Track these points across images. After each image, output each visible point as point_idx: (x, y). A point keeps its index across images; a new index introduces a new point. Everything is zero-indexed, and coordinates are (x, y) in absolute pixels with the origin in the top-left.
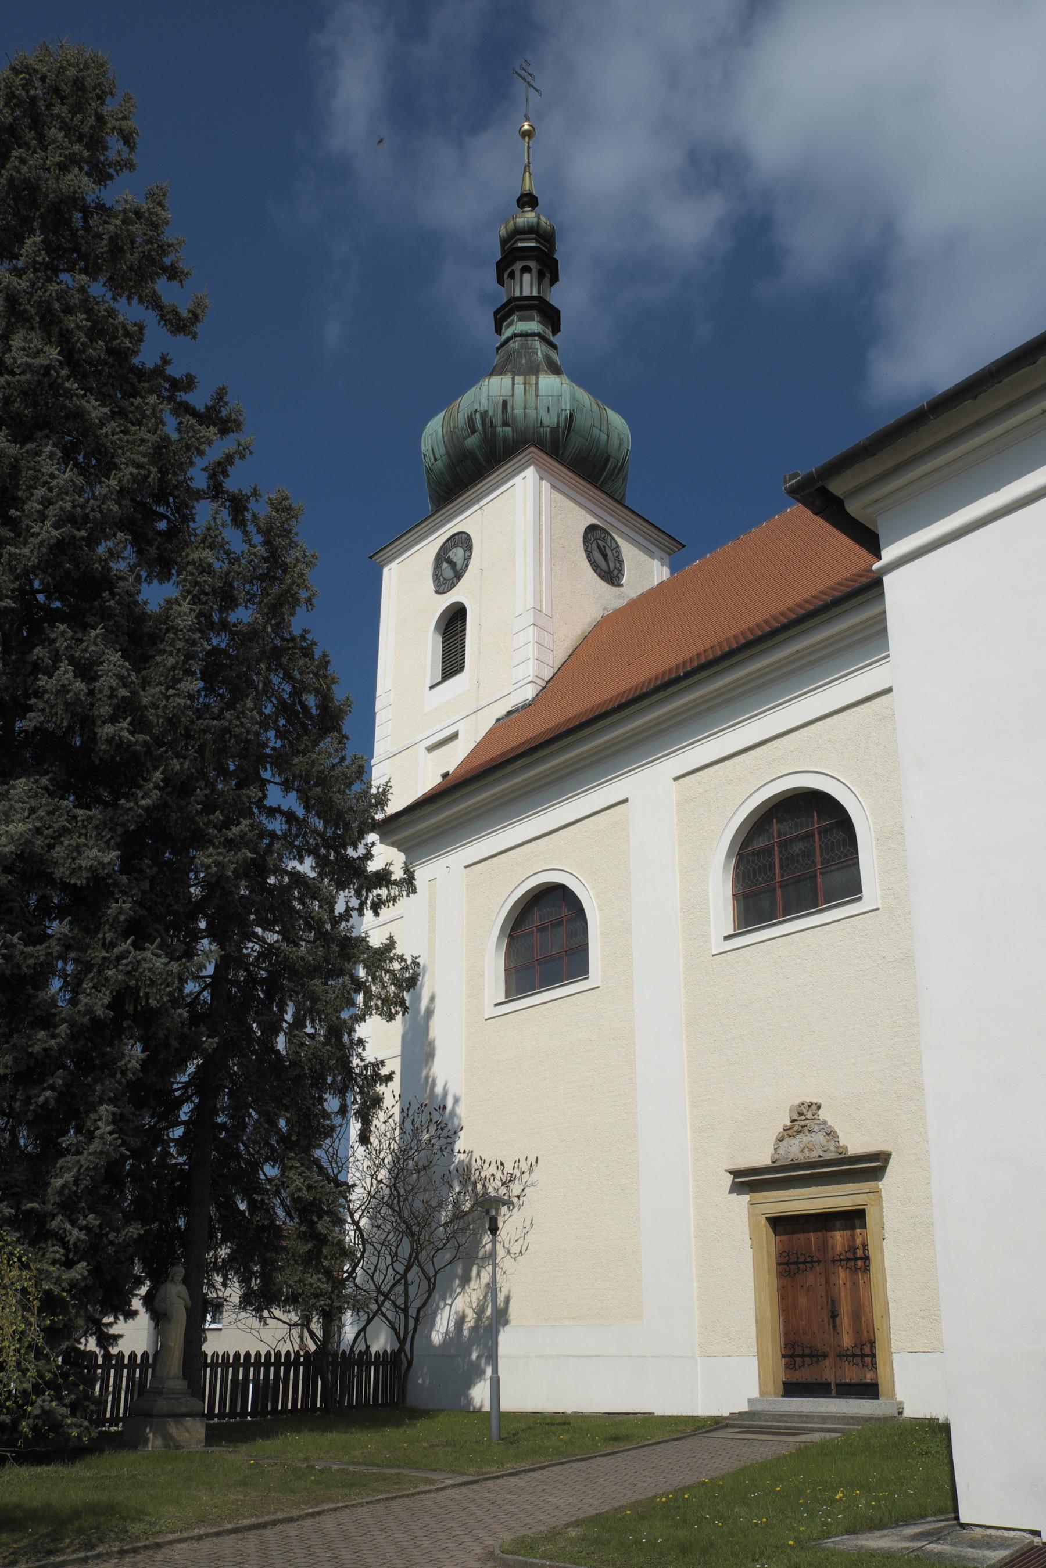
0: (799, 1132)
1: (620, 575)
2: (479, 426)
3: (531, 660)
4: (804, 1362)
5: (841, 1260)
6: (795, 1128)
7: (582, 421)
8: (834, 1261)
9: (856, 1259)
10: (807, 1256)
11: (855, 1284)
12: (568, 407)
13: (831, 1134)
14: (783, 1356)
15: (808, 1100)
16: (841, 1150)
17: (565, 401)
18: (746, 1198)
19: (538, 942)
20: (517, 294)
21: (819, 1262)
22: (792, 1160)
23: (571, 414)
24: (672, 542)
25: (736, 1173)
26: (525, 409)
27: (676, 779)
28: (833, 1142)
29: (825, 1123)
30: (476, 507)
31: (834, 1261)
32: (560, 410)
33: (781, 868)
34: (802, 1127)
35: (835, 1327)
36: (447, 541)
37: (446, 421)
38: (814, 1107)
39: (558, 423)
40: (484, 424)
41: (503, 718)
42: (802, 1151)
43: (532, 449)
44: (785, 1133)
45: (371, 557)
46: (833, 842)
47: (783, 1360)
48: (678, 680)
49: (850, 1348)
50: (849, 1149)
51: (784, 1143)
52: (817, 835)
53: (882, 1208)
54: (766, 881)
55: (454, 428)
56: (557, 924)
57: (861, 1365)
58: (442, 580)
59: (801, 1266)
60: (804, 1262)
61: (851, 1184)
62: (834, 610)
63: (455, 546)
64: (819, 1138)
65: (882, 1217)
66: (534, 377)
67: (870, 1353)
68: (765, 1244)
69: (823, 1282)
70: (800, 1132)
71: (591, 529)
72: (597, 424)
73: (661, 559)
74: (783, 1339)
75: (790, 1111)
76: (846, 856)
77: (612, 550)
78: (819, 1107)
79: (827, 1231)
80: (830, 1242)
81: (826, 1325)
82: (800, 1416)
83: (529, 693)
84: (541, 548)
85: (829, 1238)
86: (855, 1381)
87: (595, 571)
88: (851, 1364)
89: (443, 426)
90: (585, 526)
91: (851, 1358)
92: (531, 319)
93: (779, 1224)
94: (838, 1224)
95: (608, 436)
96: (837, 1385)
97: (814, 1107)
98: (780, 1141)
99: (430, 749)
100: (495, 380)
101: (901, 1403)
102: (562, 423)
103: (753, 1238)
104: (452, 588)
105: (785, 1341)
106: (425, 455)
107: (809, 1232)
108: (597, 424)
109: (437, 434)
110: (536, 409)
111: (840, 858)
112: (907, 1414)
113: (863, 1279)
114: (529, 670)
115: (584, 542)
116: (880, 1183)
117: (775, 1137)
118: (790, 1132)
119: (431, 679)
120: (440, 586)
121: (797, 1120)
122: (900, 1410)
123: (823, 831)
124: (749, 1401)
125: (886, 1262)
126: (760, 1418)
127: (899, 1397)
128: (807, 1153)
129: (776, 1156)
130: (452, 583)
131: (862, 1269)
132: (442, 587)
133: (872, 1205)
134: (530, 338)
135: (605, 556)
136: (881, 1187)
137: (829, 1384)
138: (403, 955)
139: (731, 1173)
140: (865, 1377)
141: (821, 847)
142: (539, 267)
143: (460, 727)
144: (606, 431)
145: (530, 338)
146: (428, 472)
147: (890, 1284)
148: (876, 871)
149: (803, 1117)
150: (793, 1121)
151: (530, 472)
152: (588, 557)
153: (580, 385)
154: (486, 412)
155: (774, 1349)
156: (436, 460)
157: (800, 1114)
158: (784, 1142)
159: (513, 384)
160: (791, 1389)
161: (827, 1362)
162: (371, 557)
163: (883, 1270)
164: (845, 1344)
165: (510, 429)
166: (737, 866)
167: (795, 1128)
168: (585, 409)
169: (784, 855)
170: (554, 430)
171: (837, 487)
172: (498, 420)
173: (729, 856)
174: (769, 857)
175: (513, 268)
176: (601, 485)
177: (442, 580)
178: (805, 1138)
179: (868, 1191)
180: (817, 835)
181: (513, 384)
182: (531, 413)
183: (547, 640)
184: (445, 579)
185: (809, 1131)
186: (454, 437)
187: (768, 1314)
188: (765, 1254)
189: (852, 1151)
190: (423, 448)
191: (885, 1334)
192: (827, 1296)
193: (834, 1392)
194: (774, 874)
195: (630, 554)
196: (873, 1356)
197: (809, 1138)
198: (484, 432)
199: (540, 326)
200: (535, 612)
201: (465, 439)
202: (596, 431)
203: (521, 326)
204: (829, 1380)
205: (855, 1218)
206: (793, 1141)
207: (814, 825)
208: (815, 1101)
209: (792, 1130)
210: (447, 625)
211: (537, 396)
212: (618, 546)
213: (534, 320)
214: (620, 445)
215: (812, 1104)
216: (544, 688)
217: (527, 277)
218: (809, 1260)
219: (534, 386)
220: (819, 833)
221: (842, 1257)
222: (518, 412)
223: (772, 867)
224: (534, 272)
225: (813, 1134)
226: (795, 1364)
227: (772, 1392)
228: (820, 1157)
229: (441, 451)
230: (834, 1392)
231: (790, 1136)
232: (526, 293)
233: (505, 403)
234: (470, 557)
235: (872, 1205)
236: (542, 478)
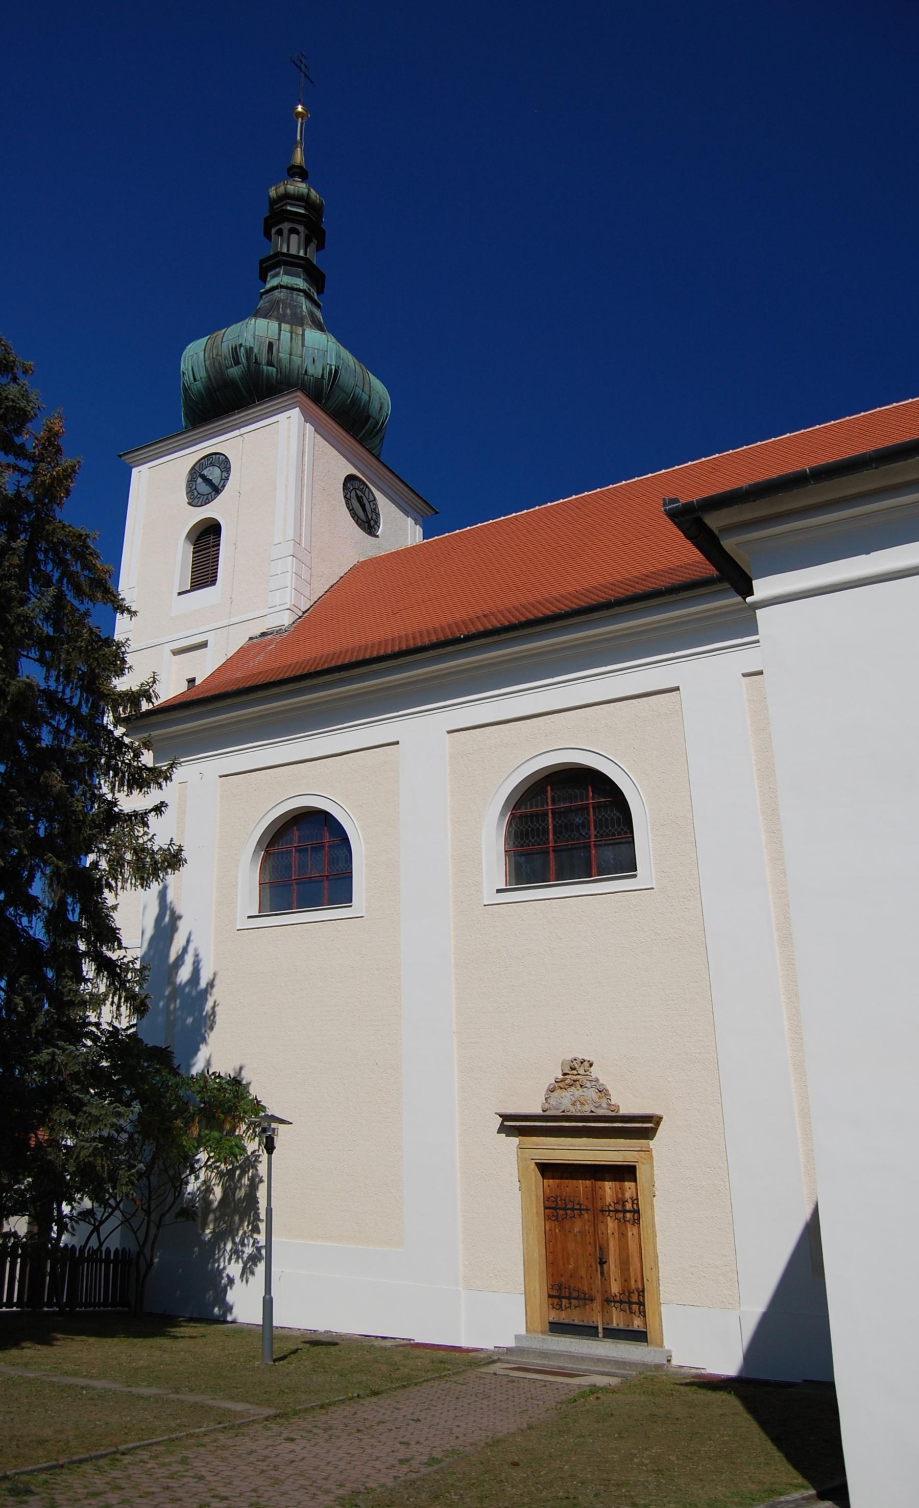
1: (376, 526)
2: (243, 360)
3: (288, 589)
4: (570, 1303)
5: (610, 1211)
6: (567, 1082)
7: (346, 379)
9: (625, 1211)
11: (623, 1235)
12: (334, 363)
13: (603, 1092)
14: (550, 1296)
15: (581, 1057)
16: (613, 1108)
17: (331, 357)
18: (515, 1141)
19: (297, 862)
20: (285, 250)
22: (564, 1112)
23: (335, 369)
24: (427, 507)
25: (505, 1117)
26: (291, 354)
27: (449, 732)
28: (605, 1099)
29: (597, 1080)
30: (236, 433)
32: (325, 364)
33: (555, 833)
34: (575, 1081)
36: (204, 458)
37: (209, 347)
38: (586, 1064)
39: (323, 375)
40: (248, 359)
41: (257, 638)
42: (573, 1104)
43: (299, 394)
44: (557, 1085)
45: (120, 456)
46: (606, 819)
47: (550, 1299)
48: (456, 641)
49: (618, 1294)
50: (621, 1108)
51: (555, 1094)
52: (591, 810)
53: (652, 1167)
54: (539, 844)
55: (217, 355)
56: (317, 848)
58: (196, 494)
59: (569, 1212)
60: (573, 1209)
62: (617, 608)
63: (212, 465)
64: (592, 1094)
65: (652, 1175)
66: (300, 328)
68: (534, 1188)
70: (572, 1085)
71: (350, 478)
72: (360, 384)
73: (415, 520)
75: (562, 1064)
76: (619, 834)
77: (369, 502)
78: (591, 1065)
79: (596, 1180)
83: (286, 619)
84: (302, 486)
87: (353, 518)
88: (619, 1309)
89: (205, 350)
90: (349, 473)
92: (297, 275)
93: (547, 1169)
95: (370, 397)
97: (586, 1064)
98: (552, 1092)
99: (176, 652)
100: (261, 323)
101: (670, 1351)
102: (326, 376)
104: (206, 504)
106: (184, 374)
108: (360, 384)
109: (198, 357)
110: (301, 357)
111: (613, 835)
112: (675, 1362)
113: (632, 1231)
114: (287, 598)
115: (344, 489)
117: (546, 1087)
118: (561, 1085)
119: (180, 585)
120: (194, 499)
121: (568, 1074)
122: (669, 1358)
123: (598, 807)
124: (517, 1337)
125: (656, 1219)
127: (667, 1345)
128: (579, 1106)
129: (547, 1106)
130: (207, 499)
131: (631, 1222)
132: (196, 500)
134: (296, 292)
135: (363, 506)
138: (180, 917)
139: (501, 1116)
141: (595, 821)
142: (306, 232)
143: (210, 637)
144: (368, 393)
145: (296, 292)
146: (185, 389)
147: (659, 1240)
148: (652, 854)
149: (575, 1072)
150: (565, 1074)
151: (296, 413)
152: (347, 504)
153: (345, 347)
154: (251, 348)
155: (540, 1288)
156: (195, 380)
157: (573, 1069)
158: (555, 1092)
159: (280, 330)
160: (557, 1328)
162: (120, 456)
163: (653, 1225)
165: (275, 369)
166: (510, 824)
167: (567, 1082)
168: (349, 369)
169: (557, 822)
170: (319, 381)
171: (714, 521)
172: (263, 359)
173: (503, 814)
174: (543, 821)
175: (281, 226)
176: (360, 439)
177: (196, 494)
178: (577, 1092)
179: (639, 1149)
180: (591, 810)
181: (280, 330)
182: (297, 361)
183: (305, 574)
184: (199, 494)
185: (581, 1086)
186: (217, 364)
187: (536, 1255)
188: (534, 1198)
189: (623, 1111)
190: (183, 367)
191: (655, 1284)
192: (595, 1243)
193: (600, 1335)
194: (548, 839)
195: (386, 508)
196: (642, 1304)
198: (248, 366)
199: (306, 284)
200: (294, 544)
201: (227, 368)
202: (358, 390)
203: (286, 280)
205: (626, 1173)
206: (564, 1093)
207: (587, 799)
208: (587, 1058)
209: (563, 1083)
210: (198, 537)
211: (303, 345)
212: (375, 499)
213: (300, 277)
214: (381, 408)
215: (584, 1061)
216: (300, 617)
217: (294, 238)
218: (578, 1207)
219: (300, 337)
220: (593, 808)
221: (611, 1208)
222: (284, 356)
223: (546, 832)
224: (302, 234)
225: (585, 1090)
226: (561, 1304)
227: (539, 1330)
228: (592, 1112)
229: (202, 374)
230: (600, 1335)
231: (561, 1088)
232: (293, 251)
233: (271, 345)
234: (227, 479)
236: (306, 421)
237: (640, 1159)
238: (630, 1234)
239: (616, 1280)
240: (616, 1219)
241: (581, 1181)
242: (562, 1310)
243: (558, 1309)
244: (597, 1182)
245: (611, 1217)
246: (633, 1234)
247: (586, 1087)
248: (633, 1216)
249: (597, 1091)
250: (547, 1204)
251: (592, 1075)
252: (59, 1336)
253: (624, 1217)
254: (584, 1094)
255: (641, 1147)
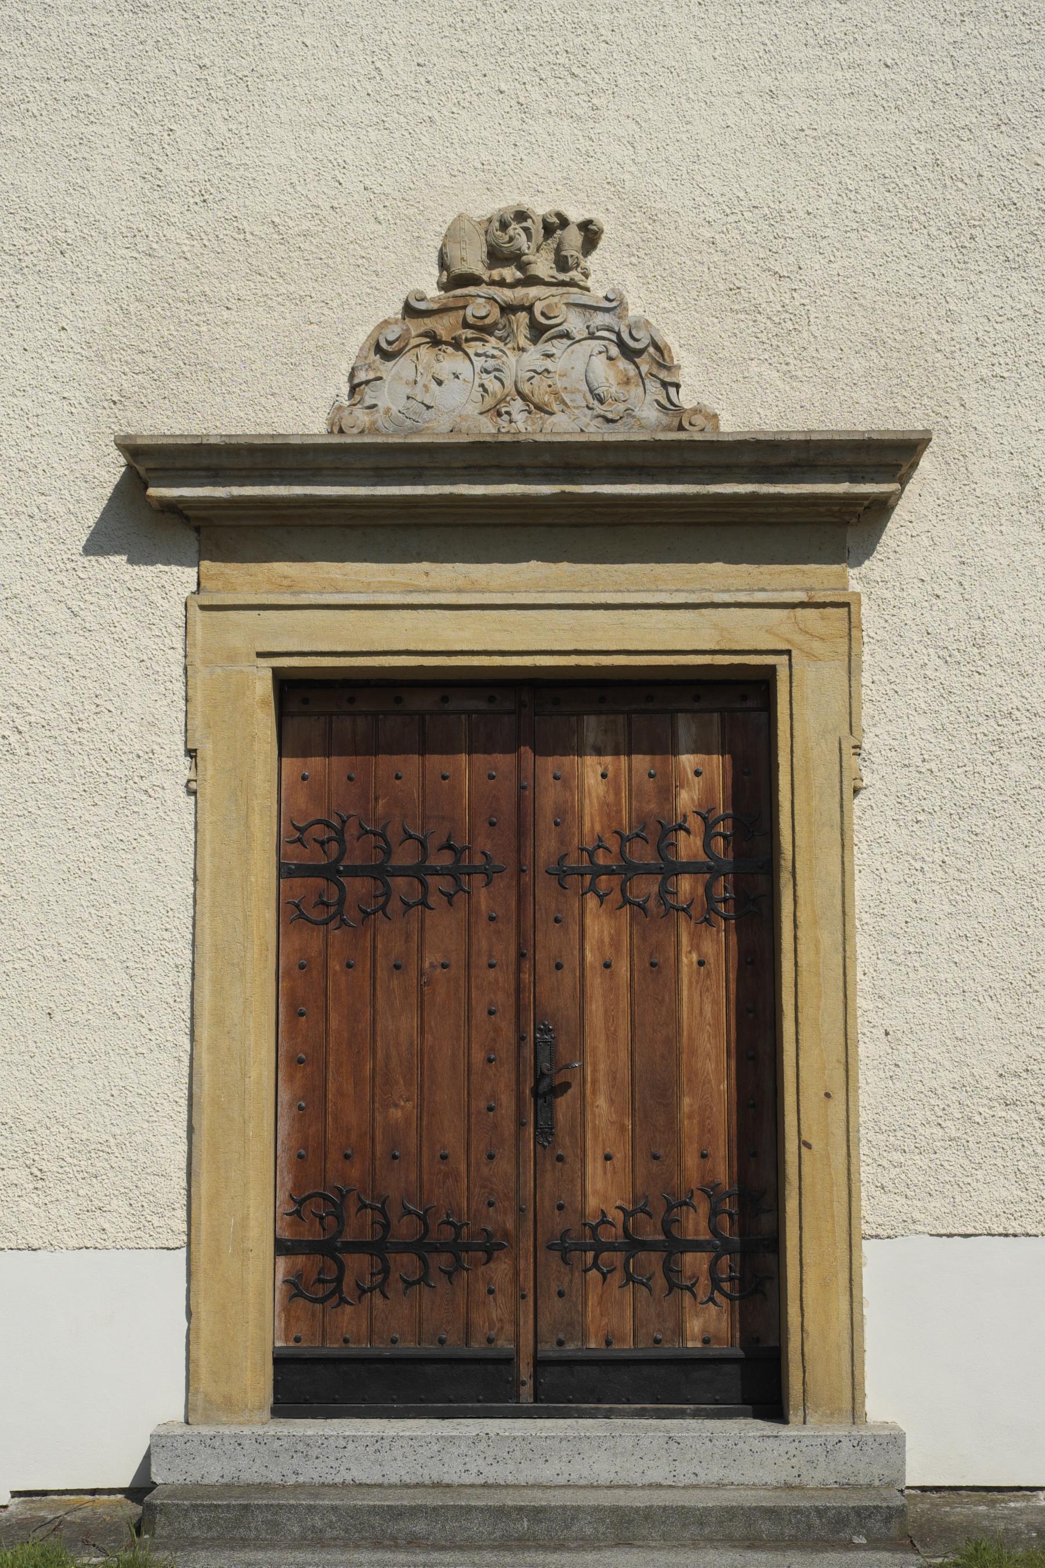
0: (483, 330)
5: (598, 871)
8: (561, 874)
10: (433, 844)
14: (281, 1247)
15: (541, 208)
21: (489, 874)
29: (614, 305)
31: (561, 874)
34: (508, 309)
35: (545, 1132)
38: (573, 238)
47: (281, 1261)
51: (403, 366)
57: (660, 1282)
59: (400, 883)
61: (718, 567)
67: (705, 1236)
69: (506, 952)
74: (287, 1180)
80: (549, 797)
81: (508, 1127)
82: (500, 1512)
85: (546, 779)
86: (625, 1346)
88: (617, 1278)
91: (618, 1258)
94: (591, 726)
96: (539, 1364)
98: (387, 356)
103: (206, 750)
105: (297, 1186)
107: (449, 748)
116: (852, 572)
118: (442, 326)
126: (274, 1526)
128: (519, 417)
133: (810, 655)
136: (854, 586)
137: (508, 1361)
140: (680, 1330)
149: (510, 273)
161: (501, 1269)
164: (593, 1203)
179: (800, 596)
197: (533, 357)
204: (504, 1345)
206: (451, 362)
218: (445, 859)
221: (601, 860)
225: (558, 347)
226: (339, 1280)
235: (810, 655)
237: (798, 638)
238: (688, 960)
239: (608, 1158)
240: (626, 901)
241: (464, 758)
242: (343, 1301)
243: (322, 1301)
244: (540, 760)
245: (601, 898)
246: (701, 963)
247: (567, 335)
248: (708, 888)
249: (614, 351)
250: (298, 856)
251: (589, 283)
252: (694, 730)
253: (664, 892)
254: (548, 364)
255: (807, 590)
